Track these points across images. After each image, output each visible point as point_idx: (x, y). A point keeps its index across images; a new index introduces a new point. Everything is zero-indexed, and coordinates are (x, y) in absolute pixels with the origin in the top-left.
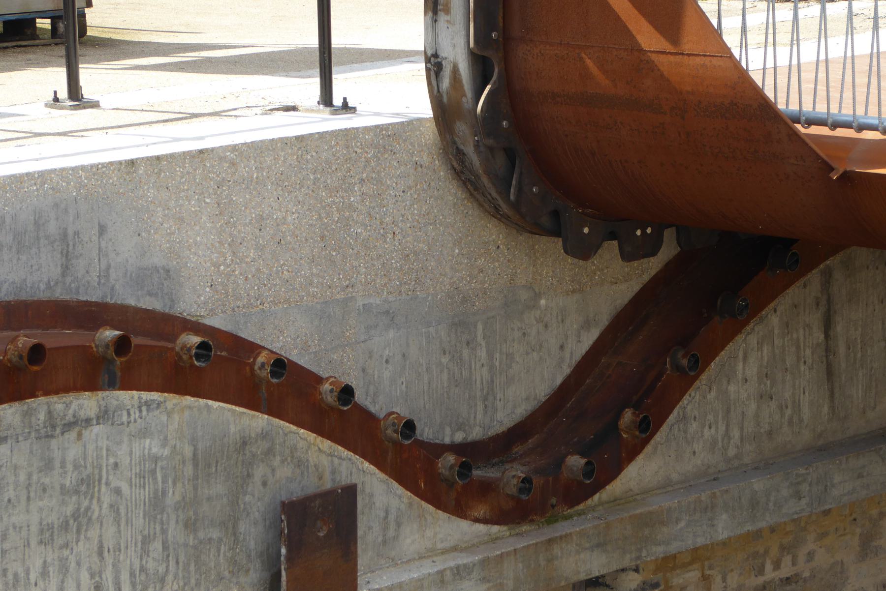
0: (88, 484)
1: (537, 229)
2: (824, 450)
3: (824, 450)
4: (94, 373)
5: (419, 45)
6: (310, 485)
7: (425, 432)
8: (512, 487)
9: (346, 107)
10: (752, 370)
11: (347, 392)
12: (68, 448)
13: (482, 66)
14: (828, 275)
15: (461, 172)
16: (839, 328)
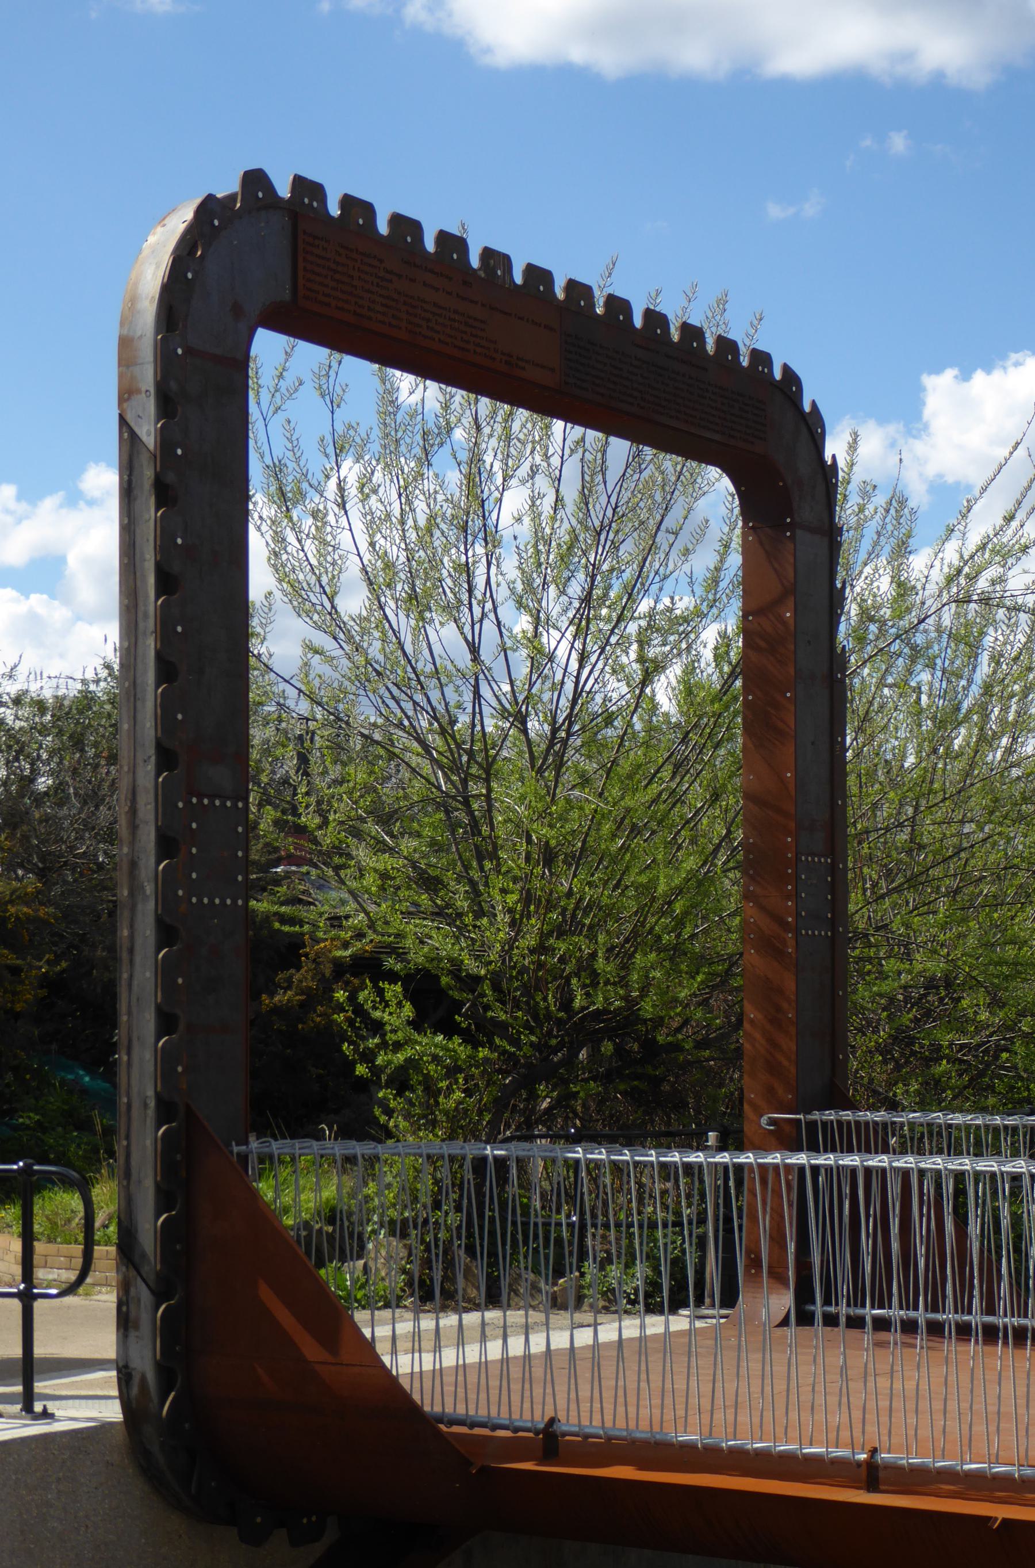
9: (46, 1415)
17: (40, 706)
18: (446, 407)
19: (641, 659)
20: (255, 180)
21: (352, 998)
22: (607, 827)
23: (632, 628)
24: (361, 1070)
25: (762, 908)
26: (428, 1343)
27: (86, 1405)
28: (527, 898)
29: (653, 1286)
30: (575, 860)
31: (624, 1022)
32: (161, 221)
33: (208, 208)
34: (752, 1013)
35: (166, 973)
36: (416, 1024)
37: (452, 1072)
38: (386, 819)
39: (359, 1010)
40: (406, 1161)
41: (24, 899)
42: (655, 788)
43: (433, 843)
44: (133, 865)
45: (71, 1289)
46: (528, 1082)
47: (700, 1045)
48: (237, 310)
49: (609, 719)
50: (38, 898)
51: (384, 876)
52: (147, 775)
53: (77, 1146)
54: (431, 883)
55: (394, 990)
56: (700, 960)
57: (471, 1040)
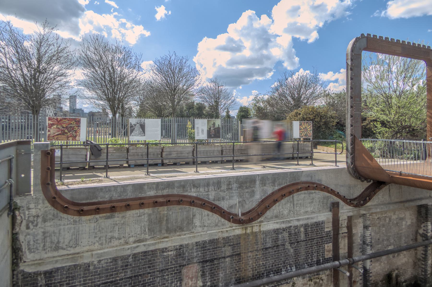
0: (313, 199)
1: (358, 179)
2: (389, 204)
3: (389, 204)
4: (314, 189)
5: (345, 161)
6: (335, 201)
7: (346, 197)
8: (355, 204)
10: (381, 195)
11: (338, 193)
12: (311, 195)
13: (352, 164)
14: (389, 186)
15: (350, 173)
16: (391, 191)
17: (336, 94)
18: (385, 57)
19: (412, 84)
20: (362, 35)
21: (373, 124)
22: (407, 104)
23: (411, 80)
24: (374, 132)
25: (429, 113)
26: (384, 162)
27: (343, 165)
28: (396, 112)
29: (415, 157)
30: (403, 108)
31: (410, 126)
32: (351, 40)
33: (357, 39)
34: (428, 125)
35: (352, 121)
36: (382, 127)
37: (386, 132)
38: (377, 104)
39: (374, 125)
40: (380, 143)
41: (334, 114)
42: (414, 99)
43: (384, 106)
44: (348, 109)
45: (340, 154)
46: (397, 133)
47: (421, 129)
48: (360, 49)
49: (407, 91)
50: (336, 114)
51: (377, 110)
52: (349, 99)
53: (342, 139)
54: (383, 111)
55: (379, 123)
56: (420, 119)
57: (388, 128)
